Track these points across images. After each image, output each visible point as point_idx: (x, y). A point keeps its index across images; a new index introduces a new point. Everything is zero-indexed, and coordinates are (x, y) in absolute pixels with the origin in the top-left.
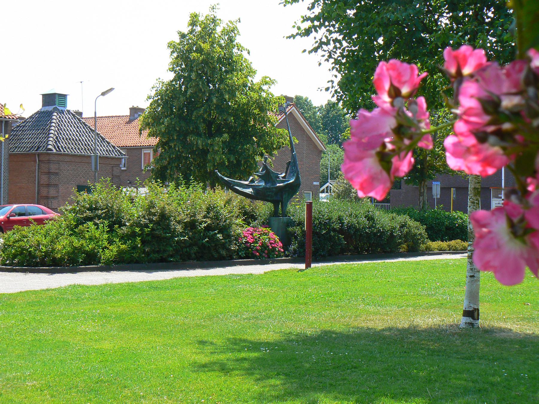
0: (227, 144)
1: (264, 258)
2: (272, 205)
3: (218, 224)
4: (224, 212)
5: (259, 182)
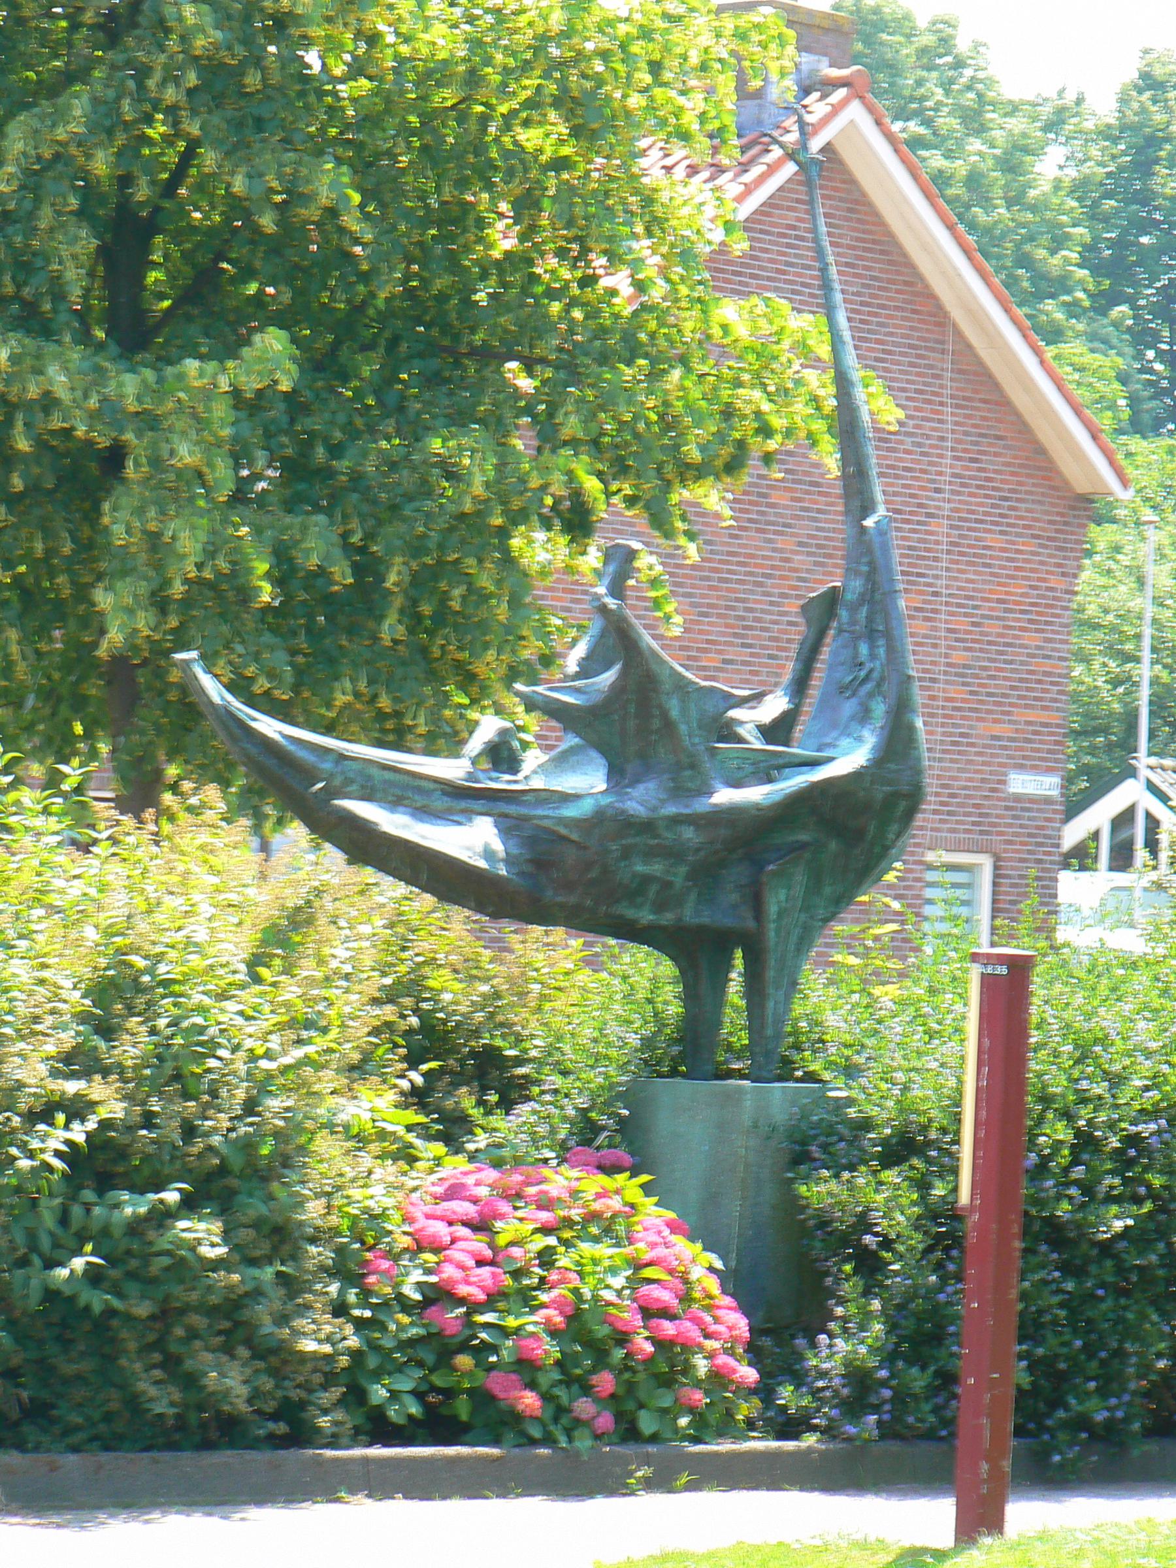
0: (277, 412)
1: (584, 1443)
2: (668, 968)
3: (189, 1131)
4: (246, 1031)
5: (562, 761)
